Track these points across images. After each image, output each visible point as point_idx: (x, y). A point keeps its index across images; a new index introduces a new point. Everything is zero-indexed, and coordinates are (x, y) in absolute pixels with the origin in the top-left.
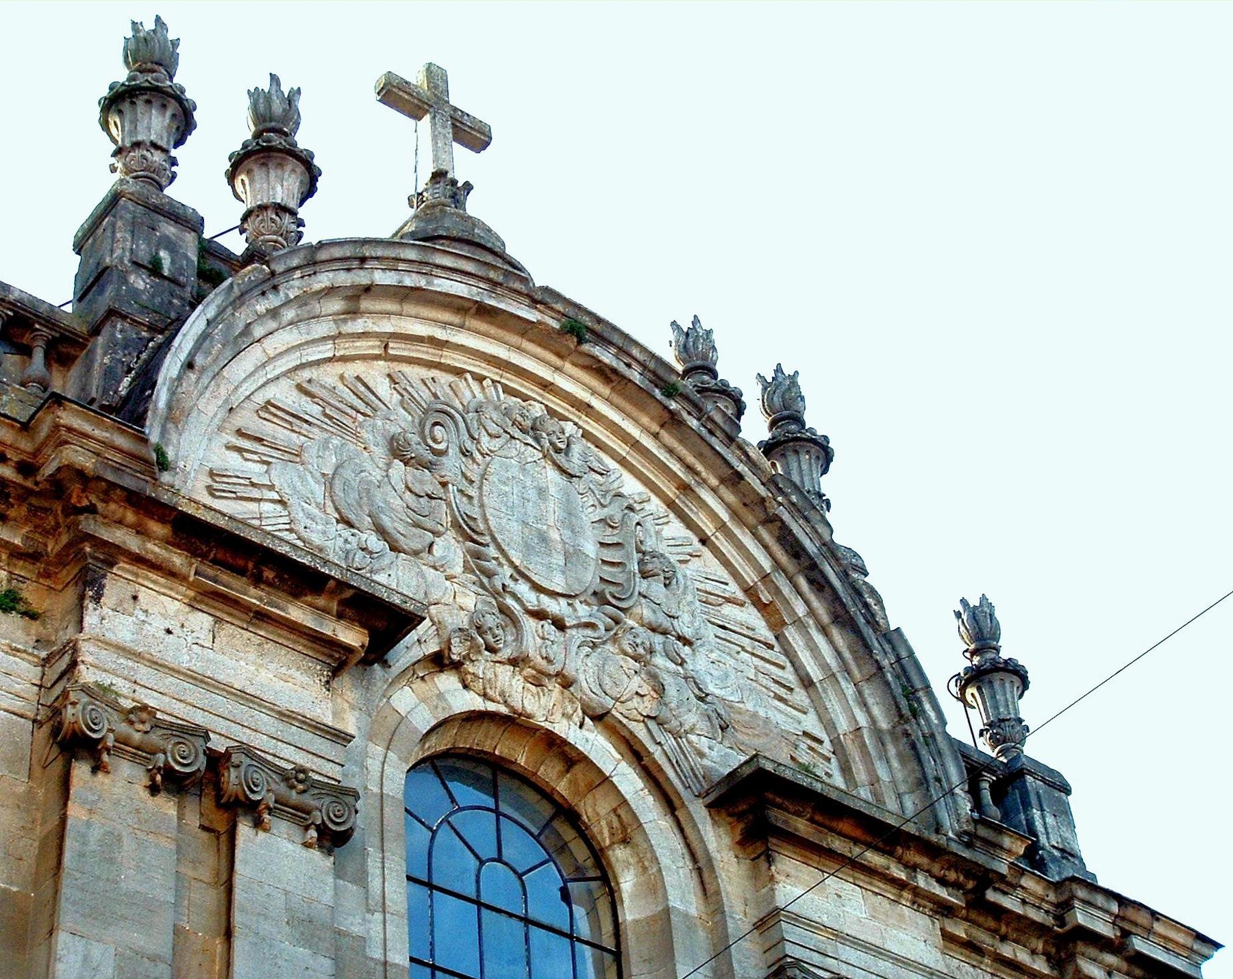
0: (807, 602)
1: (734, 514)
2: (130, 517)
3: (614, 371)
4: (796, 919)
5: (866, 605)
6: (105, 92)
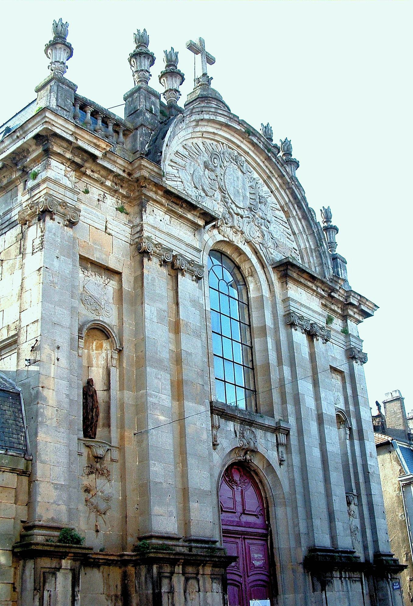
0: (296, 212)
1: (280, 185)
2: (154, 189)
3: (256, 144)
4: (293, 300)
5: (312, 214)
6: (132, 52)
